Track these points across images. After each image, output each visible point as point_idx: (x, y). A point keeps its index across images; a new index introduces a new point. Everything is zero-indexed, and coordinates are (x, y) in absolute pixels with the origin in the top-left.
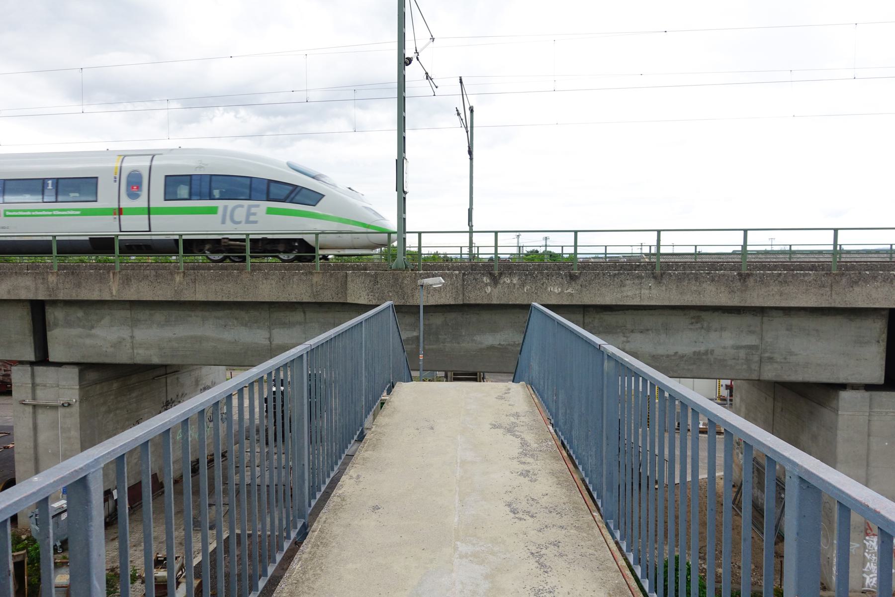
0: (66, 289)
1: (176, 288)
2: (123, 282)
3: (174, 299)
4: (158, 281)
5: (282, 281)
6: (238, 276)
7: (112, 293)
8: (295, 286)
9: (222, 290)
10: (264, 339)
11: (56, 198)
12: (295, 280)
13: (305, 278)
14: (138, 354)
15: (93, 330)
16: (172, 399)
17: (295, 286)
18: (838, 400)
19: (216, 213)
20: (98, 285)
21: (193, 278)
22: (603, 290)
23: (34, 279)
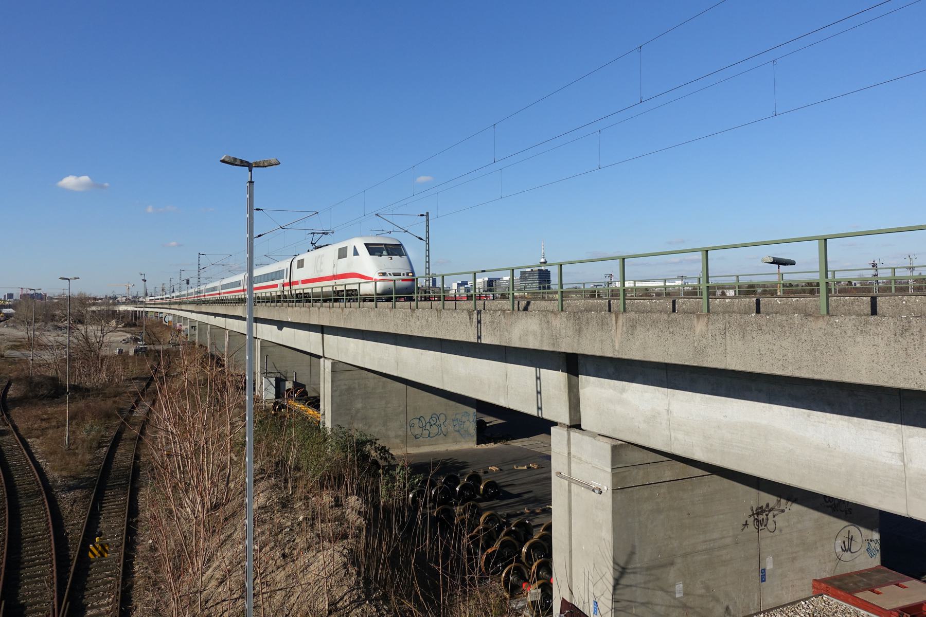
0: (568, 337)
1: (696, 344)
4: (671, 330)
5: (901, 339)
6: (802, 325)
7: (614, 346)
9: (772, 352)
10: (890, 455)
14: (676, 439)
15: (624, 394)
16: (768, 505)
19: (278, 287)
20: (599, 333)
21: (722, 326)
23: (539, 322)
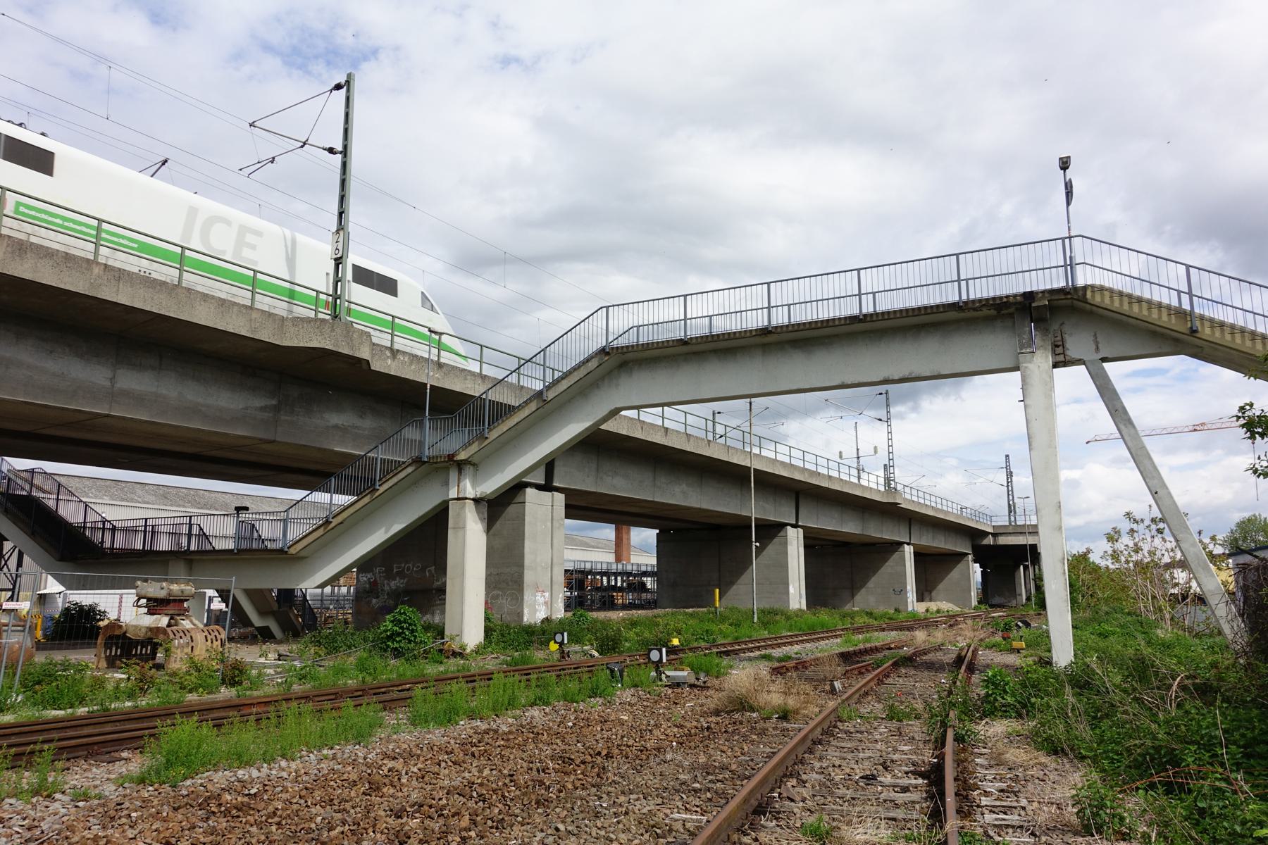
2: (13, 252)
3: (87, 293)
8: (234, 317)
11: (797, 520)
12: (234, 310)
13: (244, 311)
17: (234, 317)
18: (525, 495)
22: (456, 380)
